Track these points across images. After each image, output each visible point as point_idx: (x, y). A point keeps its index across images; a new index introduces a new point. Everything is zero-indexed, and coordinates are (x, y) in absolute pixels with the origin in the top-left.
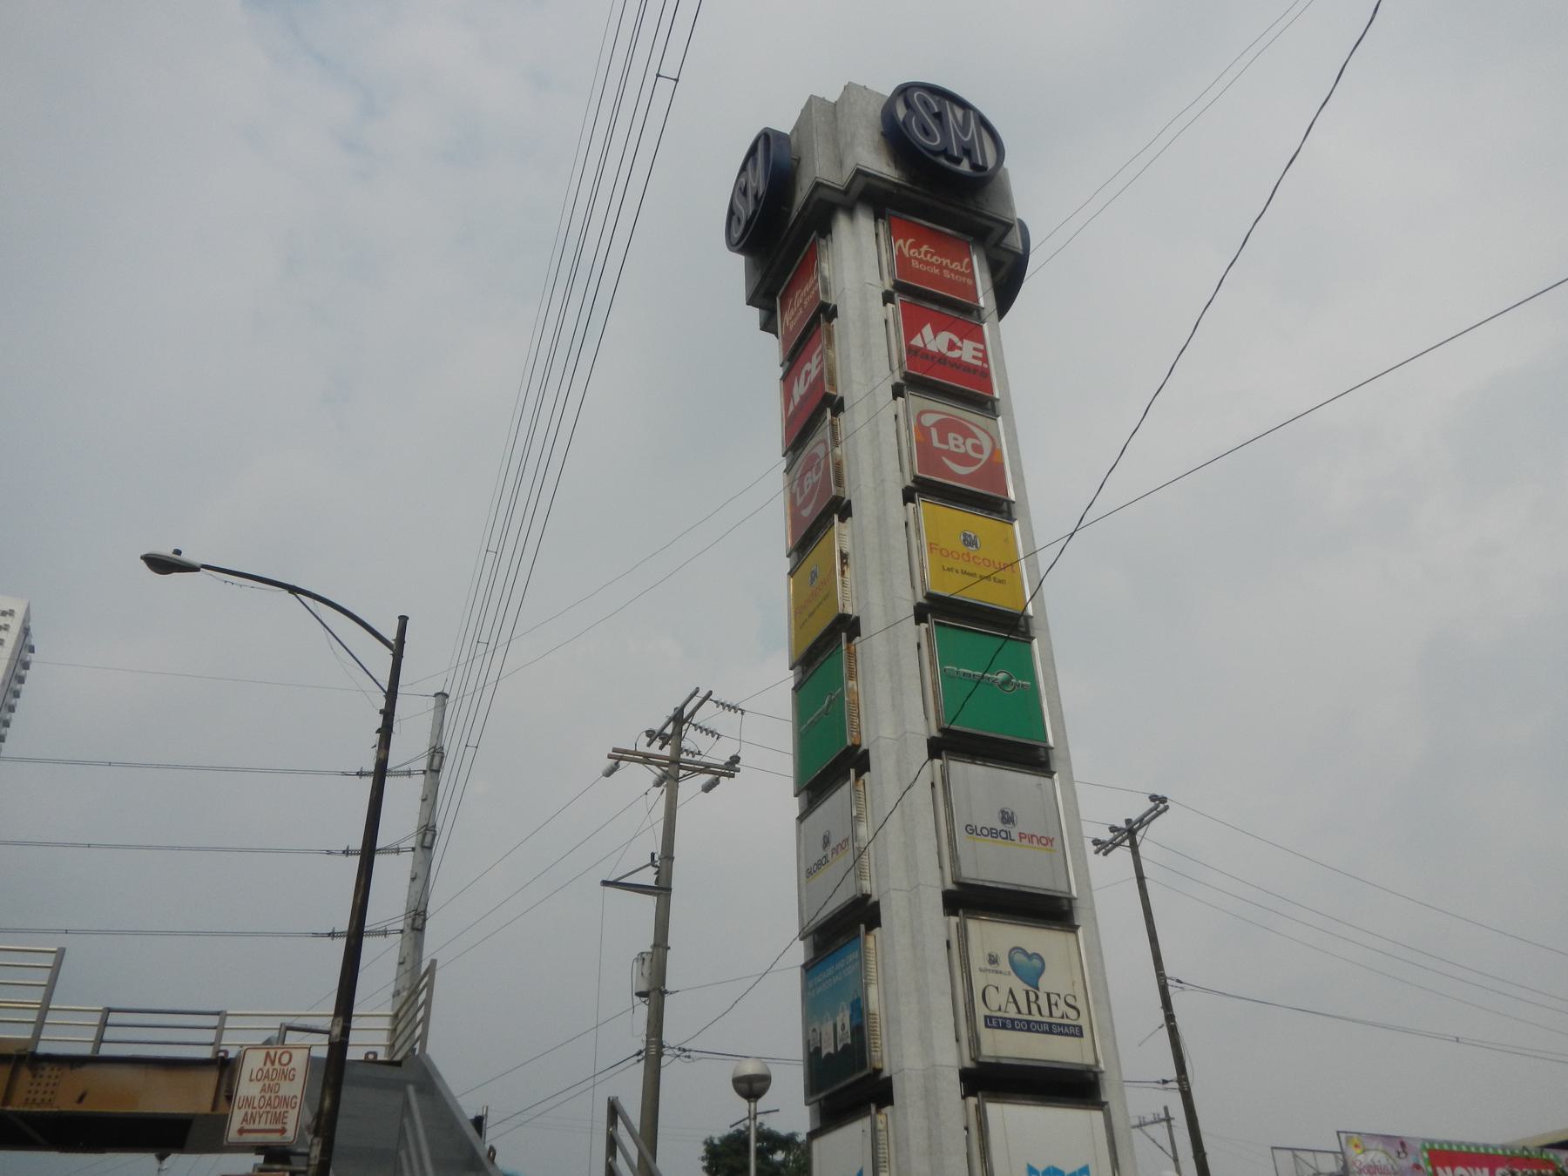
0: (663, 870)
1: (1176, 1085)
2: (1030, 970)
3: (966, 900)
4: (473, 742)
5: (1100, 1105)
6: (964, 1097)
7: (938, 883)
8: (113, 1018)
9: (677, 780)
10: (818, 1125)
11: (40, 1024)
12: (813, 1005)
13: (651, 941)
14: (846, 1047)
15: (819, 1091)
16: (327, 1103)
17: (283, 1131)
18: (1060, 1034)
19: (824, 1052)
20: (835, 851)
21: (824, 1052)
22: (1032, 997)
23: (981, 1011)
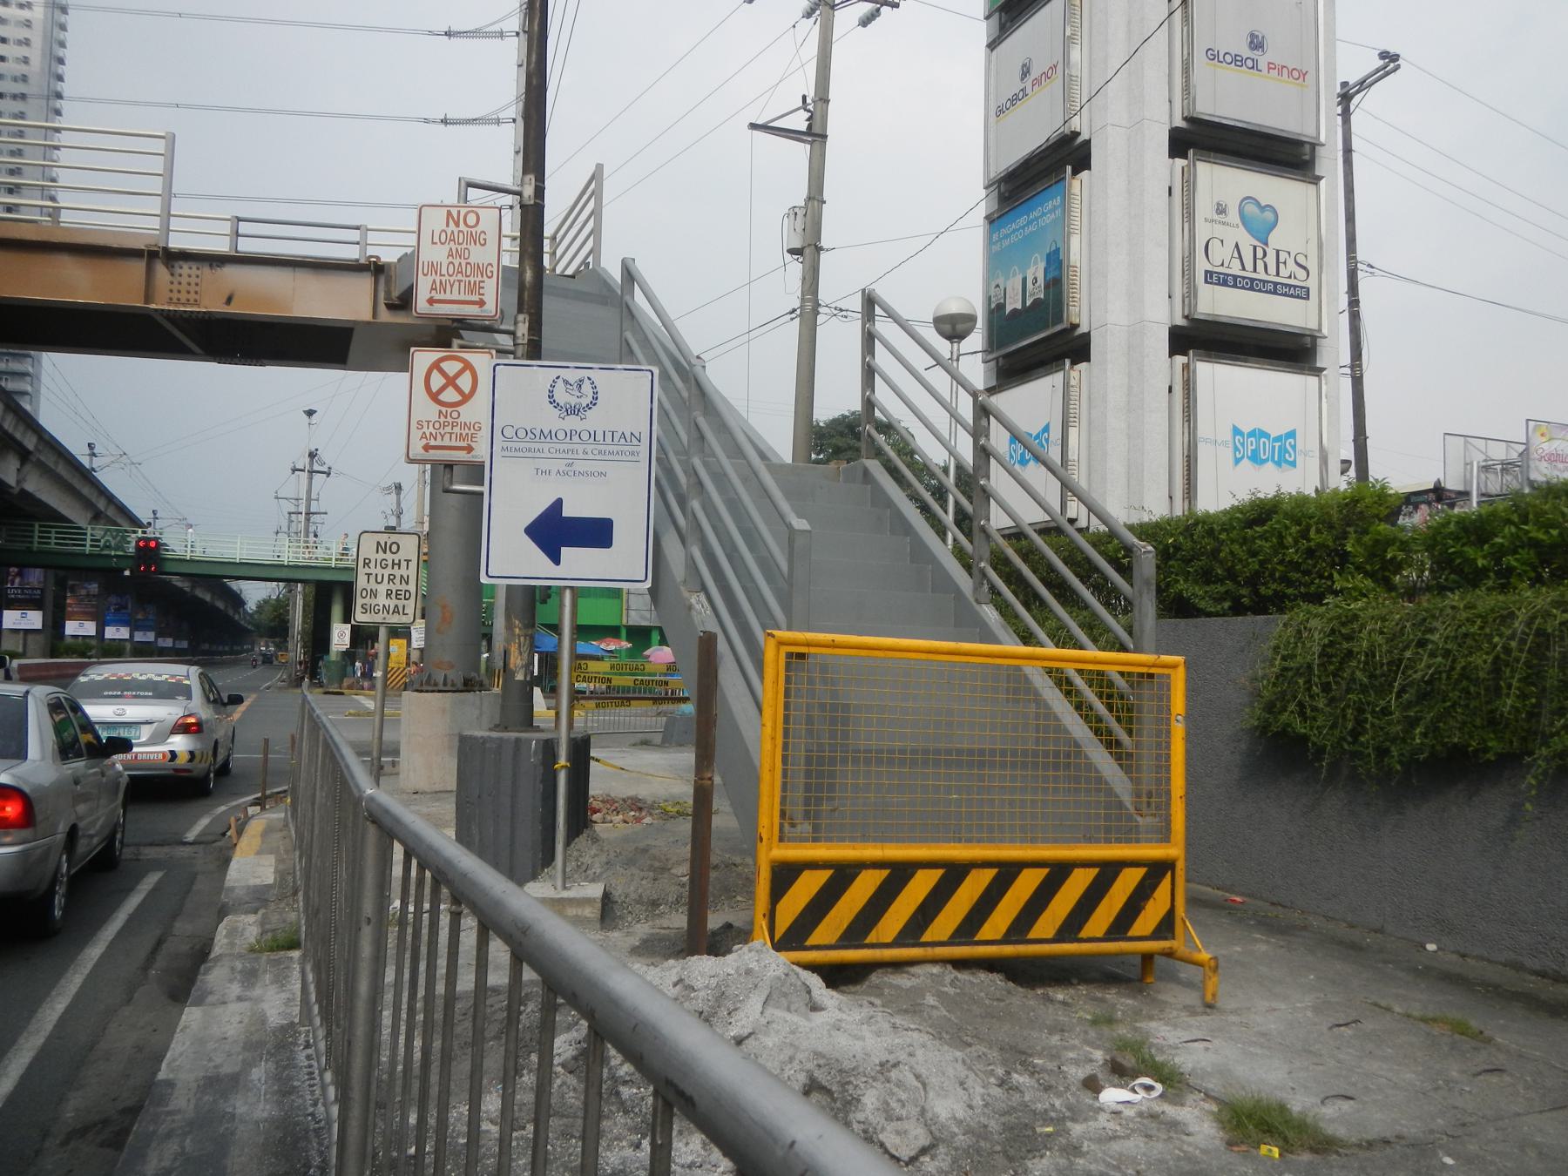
0: (817, 117)
1: (1348, 371)
2: (1261, 223)
3: (1198, 139)
5: (1317, 372)
6: (1171, 354)
7: (1166, 118)
8: (244, 228)
10: (993, 383)
12: (997, 261)
13: (804, 193)
14: (1037, 302)
15: (1000, 346)
16: (529, 275)
17: (481, 303)
18: (1285, 295)
19: (1008, 309)
20: (1037, 82)
21: (1008, 309)
22: (1260, 254)
23: (1202, 265)
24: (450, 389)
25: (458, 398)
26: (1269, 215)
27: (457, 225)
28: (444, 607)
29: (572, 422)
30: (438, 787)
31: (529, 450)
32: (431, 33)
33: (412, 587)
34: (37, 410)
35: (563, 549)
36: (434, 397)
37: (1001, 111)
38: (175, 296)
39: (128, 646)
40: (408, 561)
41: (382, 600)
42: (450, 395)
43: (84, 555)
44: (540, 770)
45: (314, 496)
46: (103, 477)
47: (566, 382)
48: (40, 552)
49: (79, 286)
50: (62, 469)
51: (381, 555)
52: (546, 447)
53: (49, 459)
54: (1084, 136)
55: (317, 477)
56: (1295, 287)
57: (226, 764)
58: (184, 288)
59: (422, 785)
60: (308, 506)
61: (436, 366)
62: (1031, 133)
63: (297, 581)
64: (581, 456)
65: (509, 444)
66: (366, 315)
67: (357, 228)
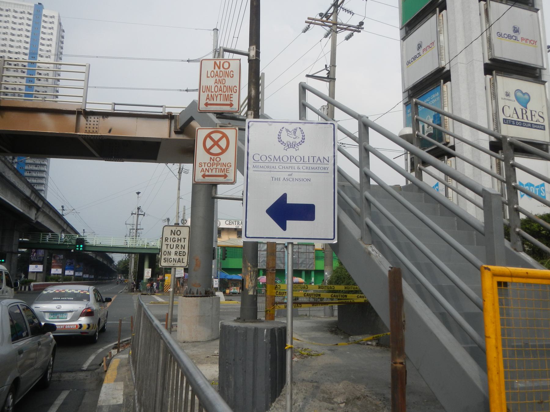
0: (332, 73)
2: (524, 100)
3: (496, 67)
4: (236, 36)
7: (482, 60)
9: (337, 32)
11: (86, 89)
16: (253, 93)
17: (231, 105)
18: (535, 128)
20: (425, 50)
22: (524, 112)
23: (502, 117)
24: (220, 143)
25: (220, 151)
26: (526, 96)
27: (219, 68)
28: (197, 260)
29: (291, 152)
30: (194, 340)
31: (268, 167)
32: (182, 61)
33: (186, 250)
34: (46, 196)
35: (288, 222)
36: (208, 151)
37: (409, 63)
38: (88, 129)
39: (73, 277)
40: (184, 239)
41: (173, 256)
42: (216, 150)
43: (57, 244)
44: (269, 346)
45: (139, 223)
46: (67, 218)
47: (287, 130)
48: (42, 244)
49: (49, 125)
50: (51, 214)
51: (173, 236)
52: (277, 165)
53: (47, 211)
54: (447, 68)
55: (140, 216)
56: (539, 125)
57: (104, 326)
58: (92, 126)
59: (187, 338)
60: (137, 227)
61: (209, 136)
62: (424, 68)
63: (132, 253)
64: (297, 170)
65: (257, 164)
66: (165, 135)
67: (162, 107)
